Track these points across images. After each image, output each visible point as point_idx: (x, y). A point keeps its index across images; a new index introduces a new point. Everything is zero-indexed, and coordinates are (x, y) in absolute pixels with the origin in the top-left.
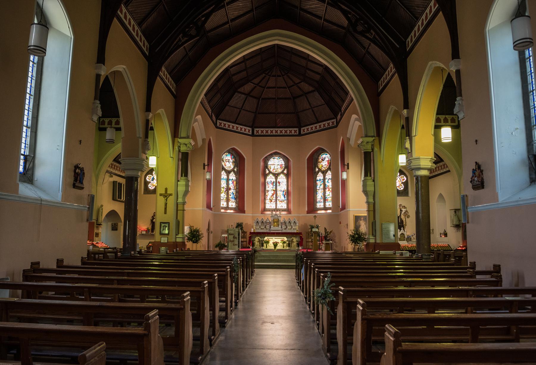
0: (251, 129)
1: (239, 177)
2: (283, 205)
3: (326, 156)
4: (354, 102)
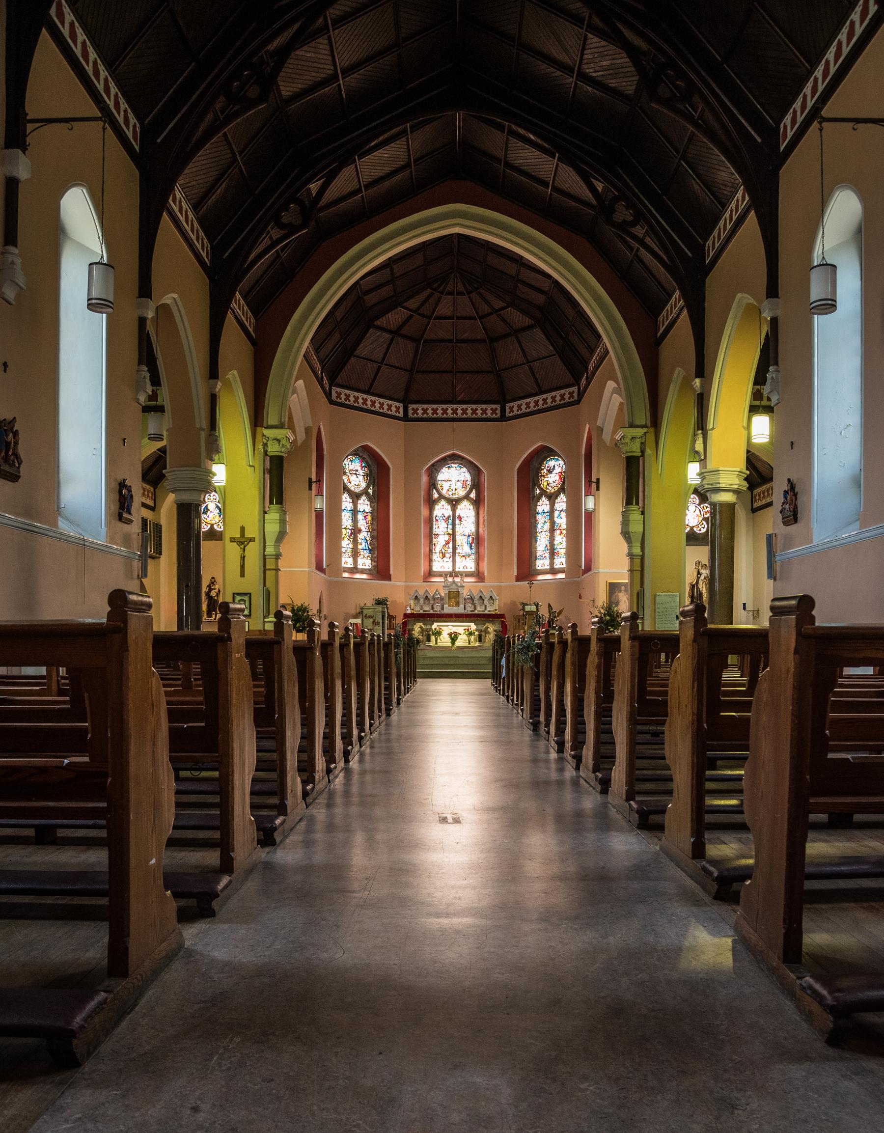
0: (402, 405)
1: (378, 506)
2: (467, 564)
3: (557, 462)
4: (610, 357)
